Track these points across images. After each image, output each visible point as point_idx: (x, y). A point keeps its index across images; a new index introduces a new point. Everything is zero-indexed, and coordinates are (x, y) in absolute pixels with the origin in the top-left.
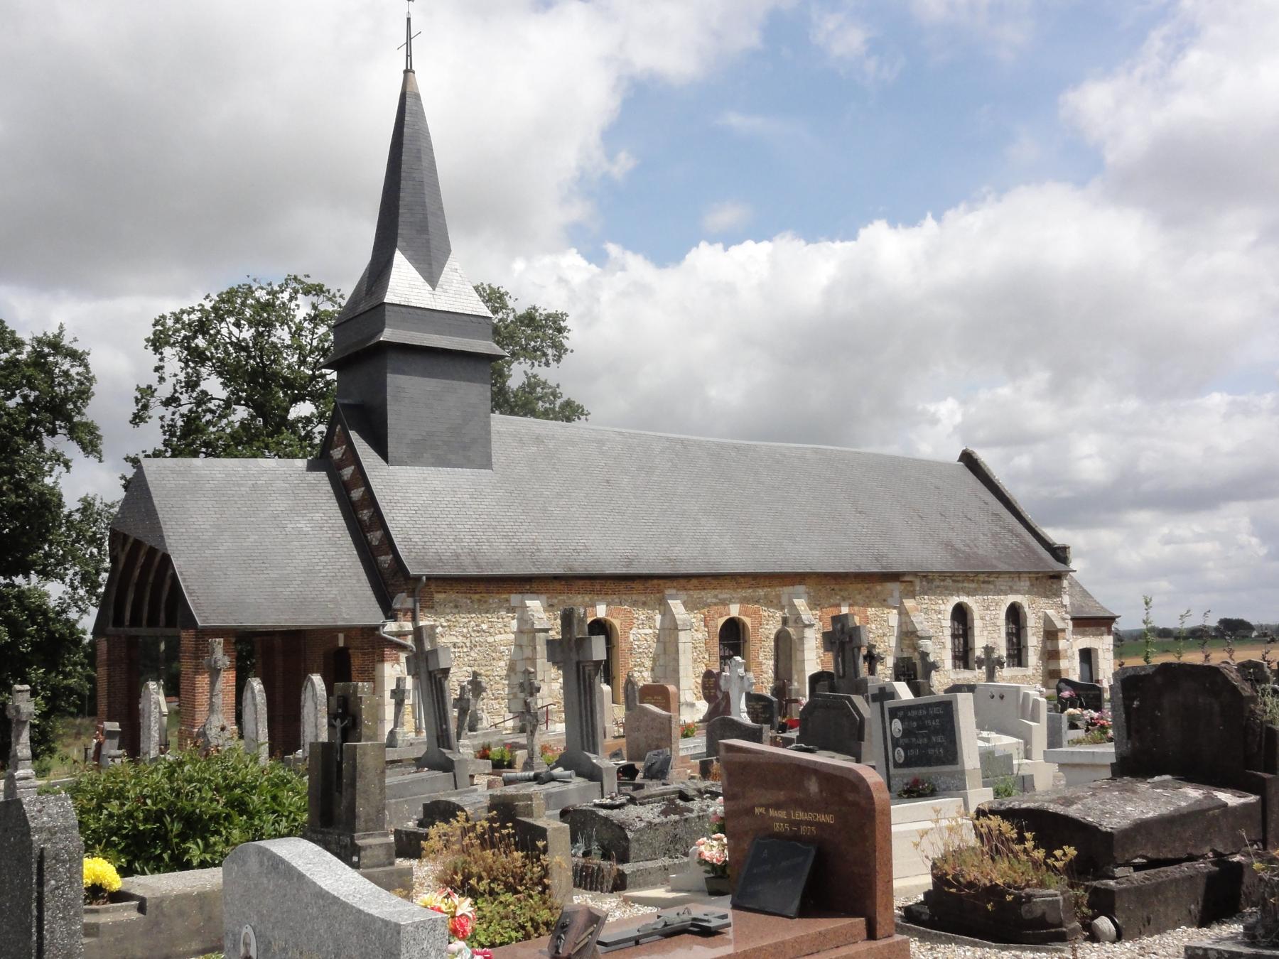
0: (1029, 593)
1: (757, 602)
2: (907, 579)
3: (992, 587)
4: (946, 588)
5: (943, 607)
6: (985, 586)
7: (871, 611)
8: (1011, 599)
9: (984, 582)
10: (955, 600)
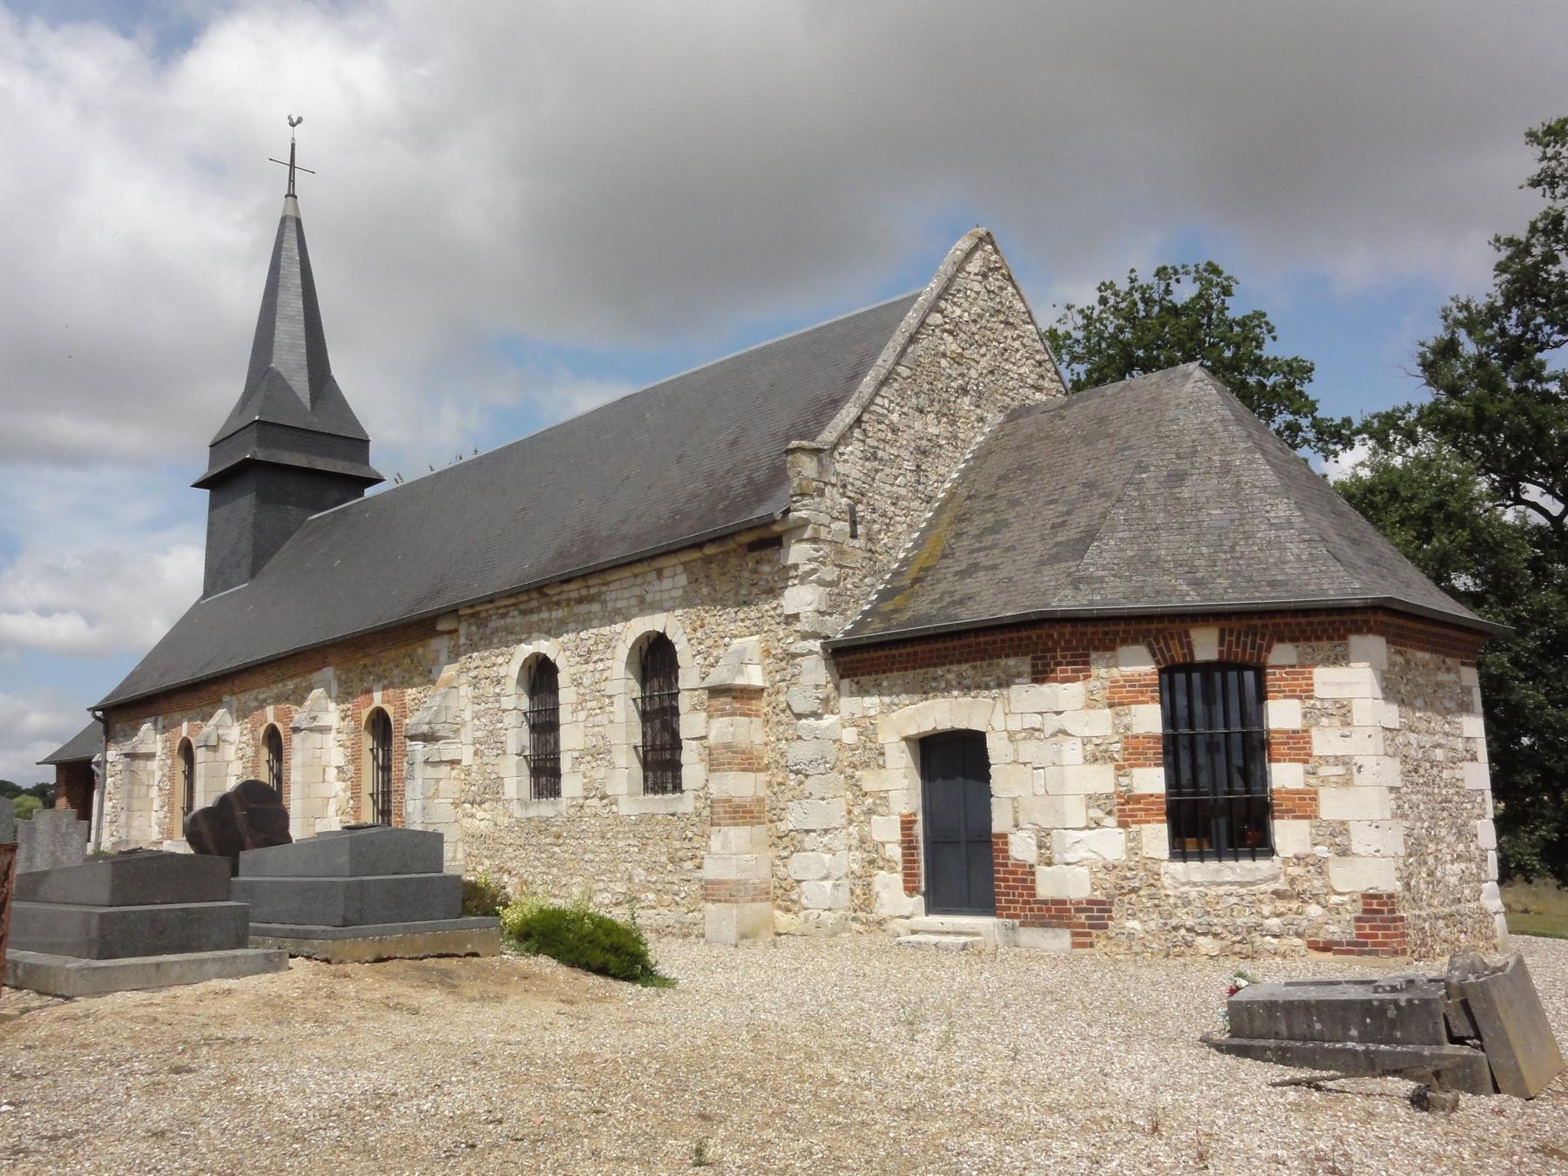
0: (687, 602)
1: (287, 700)
2: (442, 626)
3: (596, 607)
4: (509, 631)
5: (503, 671)
6: (584, 608)
7: (411, 692)
8: (526, 650)
9: (580, 601)
10: (526, 650)
